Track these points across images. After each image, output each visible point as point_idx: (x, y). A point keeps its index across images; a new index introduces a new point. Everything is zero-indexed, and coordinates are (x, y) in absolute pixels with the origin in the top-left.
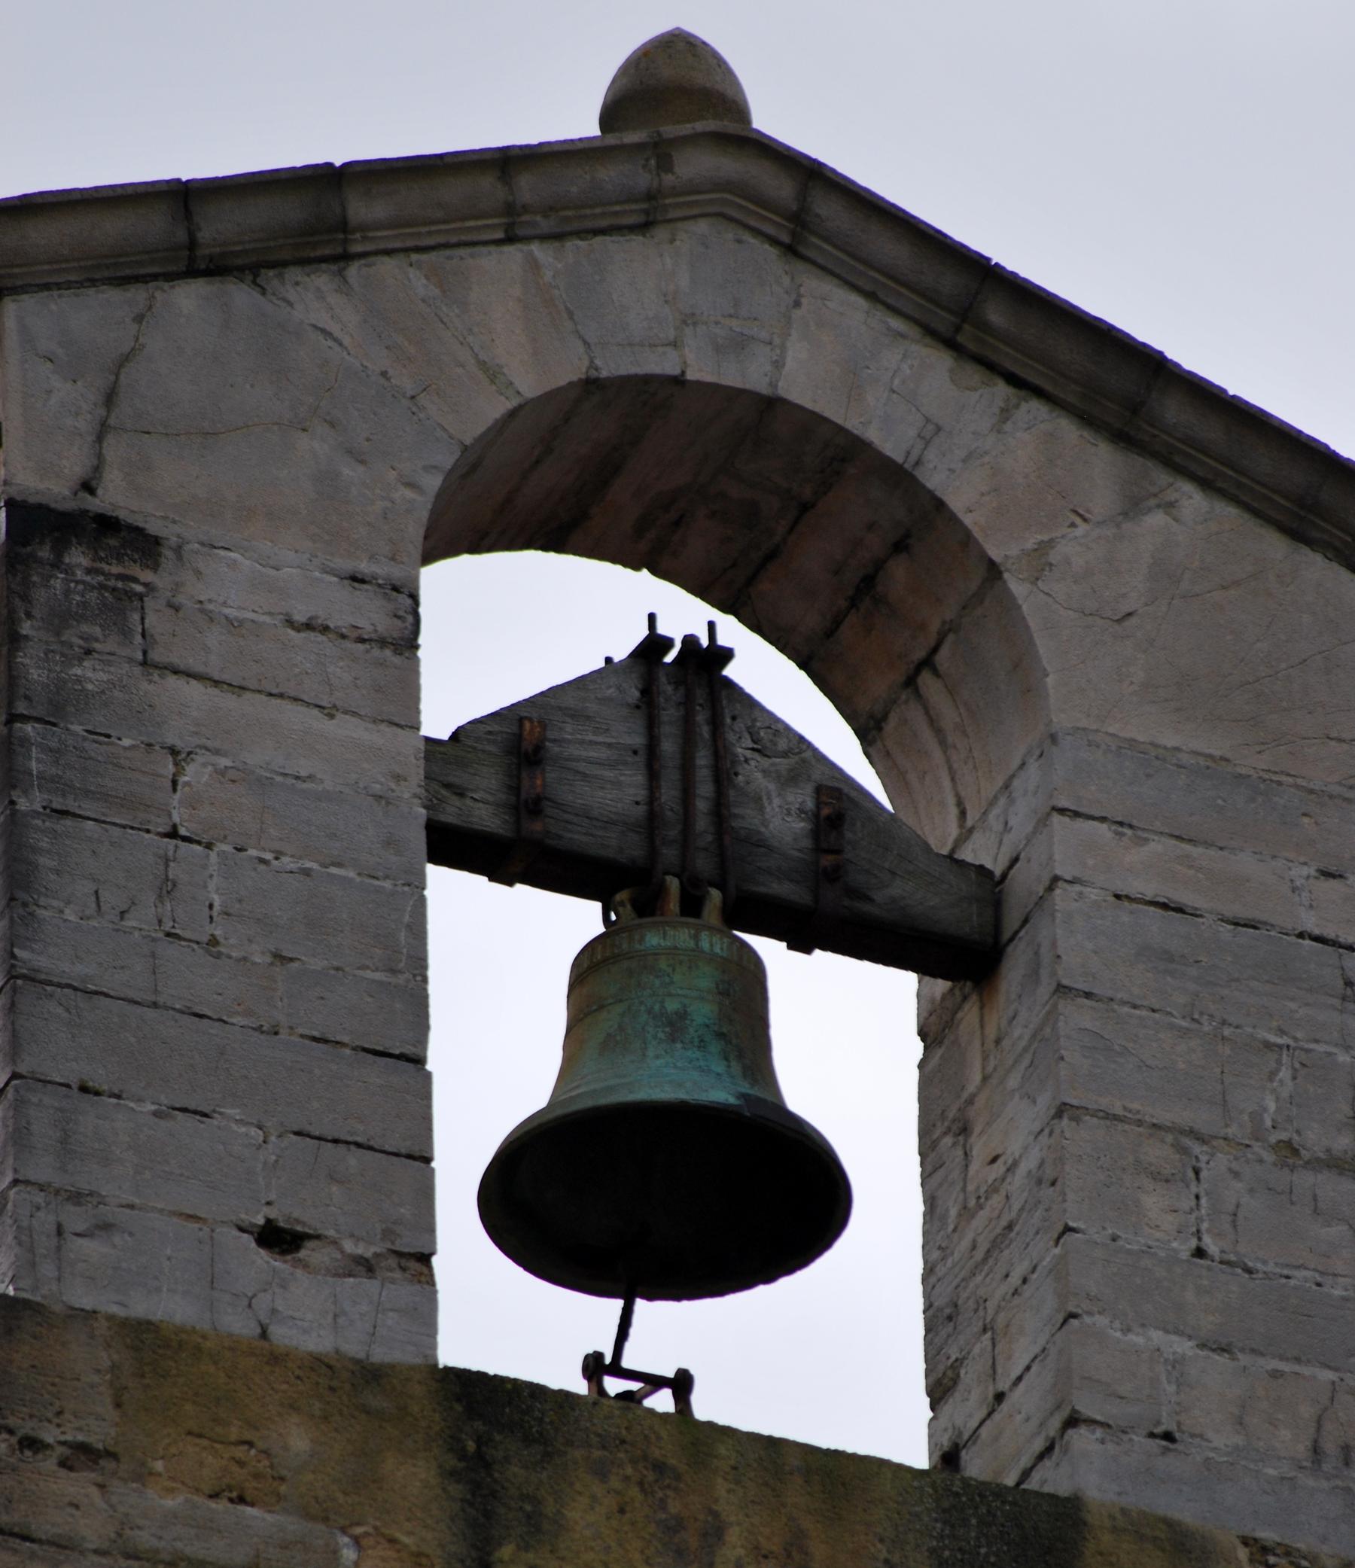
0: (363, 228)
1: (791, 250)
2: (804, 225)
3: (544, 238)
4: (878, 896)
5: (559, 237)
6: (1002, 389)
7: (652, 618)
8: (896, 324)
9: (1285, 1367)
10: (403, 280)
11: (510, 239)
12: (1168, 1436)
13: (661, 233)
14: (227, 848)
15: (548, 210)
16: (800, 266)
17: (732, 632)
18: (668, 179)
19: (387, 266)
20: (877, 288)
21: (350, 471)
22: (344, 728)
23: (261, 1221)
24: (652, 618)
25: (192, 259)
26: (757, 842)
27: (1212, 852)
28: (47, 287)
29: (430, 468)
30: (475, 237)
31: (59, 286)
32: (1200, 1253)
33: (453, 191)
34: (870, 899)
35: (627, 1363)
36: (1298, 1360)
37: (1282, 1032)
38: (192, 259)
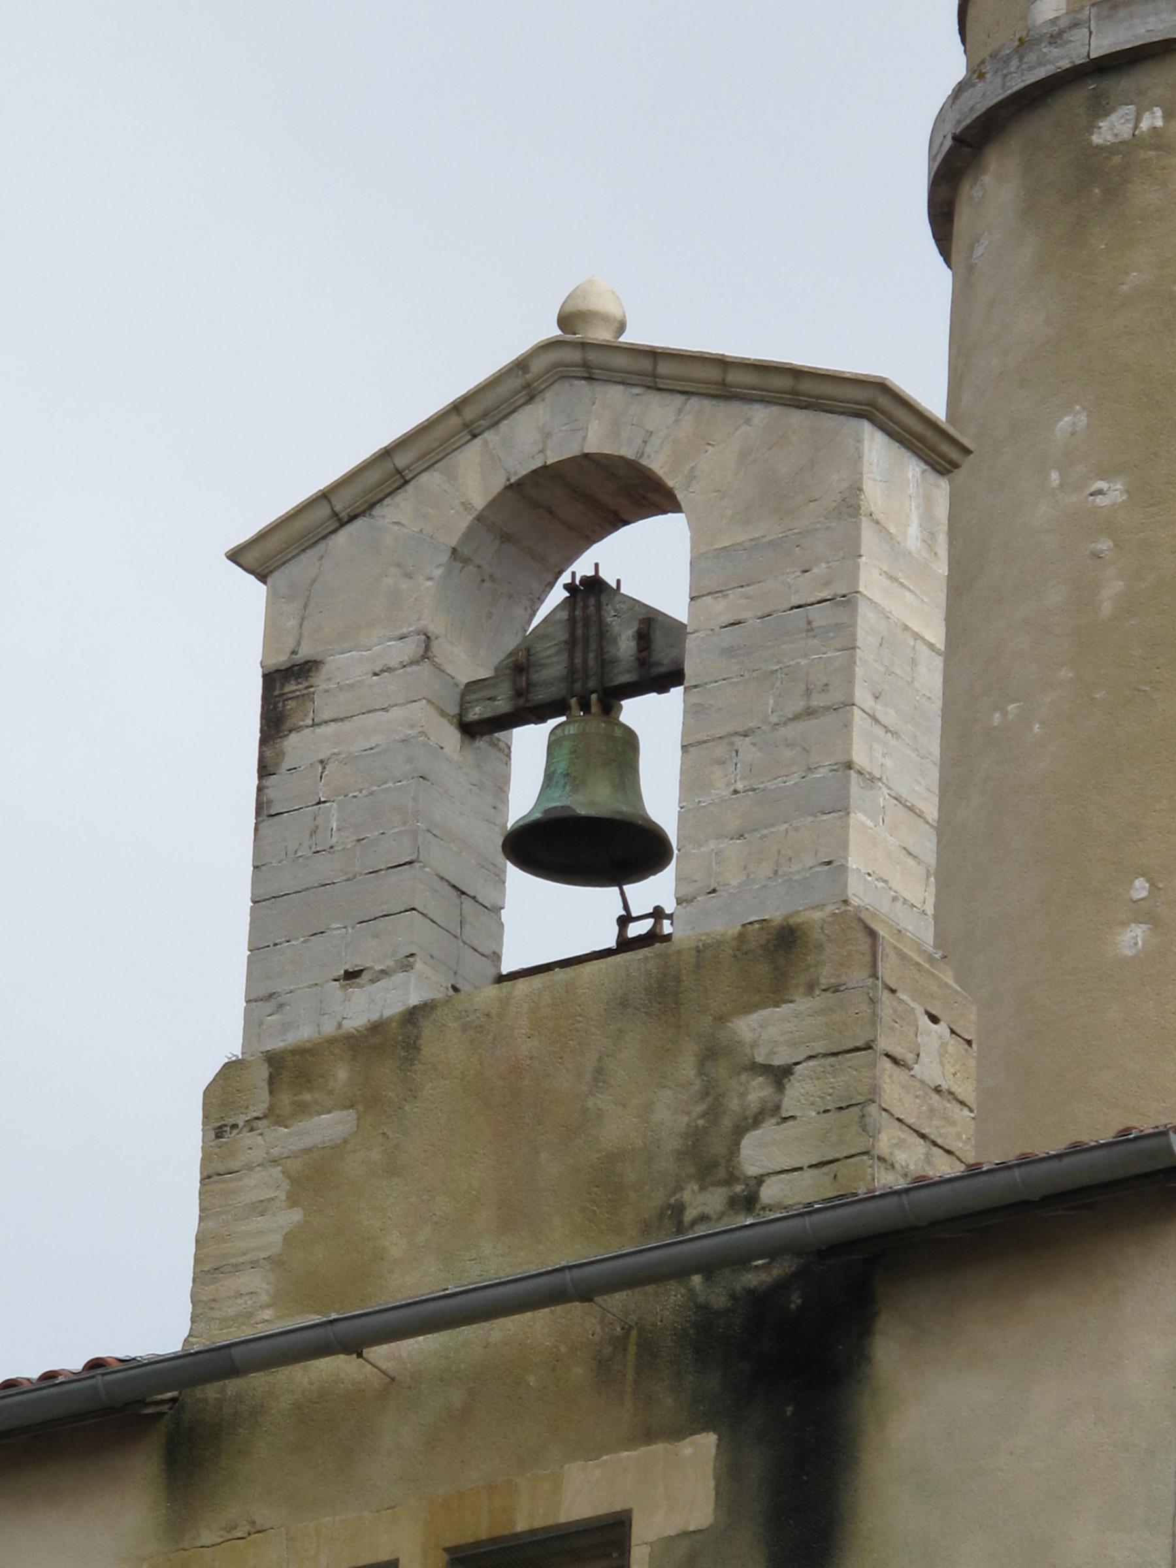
0: (408, 467)
1: (590, 379)
2: (589, 367)
3: (489, 428)
4: (666, 662)
5: (495, 424)
6: (679, 399)
7: (597, 565)
8: (637, 390)
9: (765, 832)
10: (431, 480)
11: (474, 436)
12: (714, 891)
13: (538, 399)
14: (341, 798)
15: (485, 415)
16: (595, 383)
17: (566, 578)
18: (528, 376)
19: (425, 478)
20: (623, 379)
21: (404, 585)
22: (395, 713)
23: (342, 972)
24: (597, 565)
25: (339, 520)
26: (615, 661)
27: (755, 586)
28: (284, 563)
29: (438, 566)
30: (458, 444)
31: (289, 560)
32: (736, 792)
33: (439, 432)
34: (662, 665)
35: (634, 914)
36: (772, 825)
37: (778, 662)
38: (339, 520)
